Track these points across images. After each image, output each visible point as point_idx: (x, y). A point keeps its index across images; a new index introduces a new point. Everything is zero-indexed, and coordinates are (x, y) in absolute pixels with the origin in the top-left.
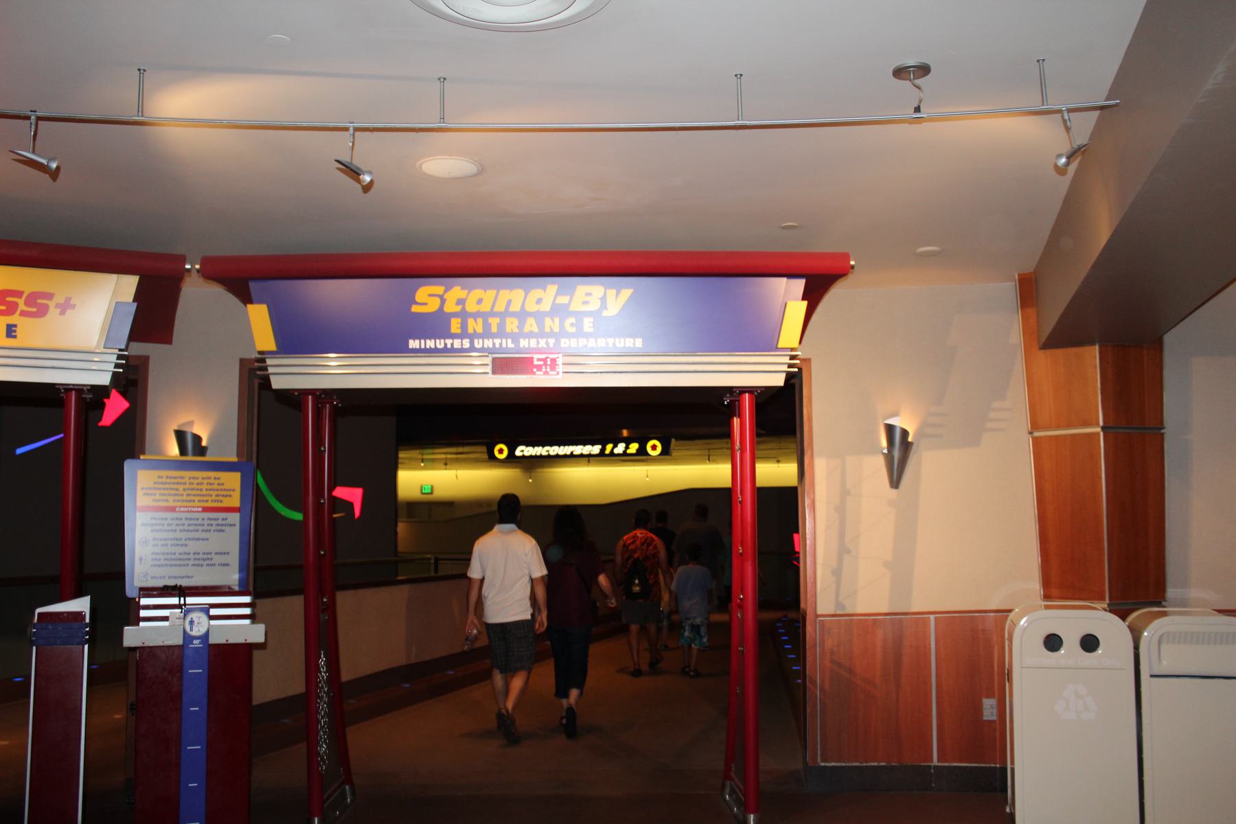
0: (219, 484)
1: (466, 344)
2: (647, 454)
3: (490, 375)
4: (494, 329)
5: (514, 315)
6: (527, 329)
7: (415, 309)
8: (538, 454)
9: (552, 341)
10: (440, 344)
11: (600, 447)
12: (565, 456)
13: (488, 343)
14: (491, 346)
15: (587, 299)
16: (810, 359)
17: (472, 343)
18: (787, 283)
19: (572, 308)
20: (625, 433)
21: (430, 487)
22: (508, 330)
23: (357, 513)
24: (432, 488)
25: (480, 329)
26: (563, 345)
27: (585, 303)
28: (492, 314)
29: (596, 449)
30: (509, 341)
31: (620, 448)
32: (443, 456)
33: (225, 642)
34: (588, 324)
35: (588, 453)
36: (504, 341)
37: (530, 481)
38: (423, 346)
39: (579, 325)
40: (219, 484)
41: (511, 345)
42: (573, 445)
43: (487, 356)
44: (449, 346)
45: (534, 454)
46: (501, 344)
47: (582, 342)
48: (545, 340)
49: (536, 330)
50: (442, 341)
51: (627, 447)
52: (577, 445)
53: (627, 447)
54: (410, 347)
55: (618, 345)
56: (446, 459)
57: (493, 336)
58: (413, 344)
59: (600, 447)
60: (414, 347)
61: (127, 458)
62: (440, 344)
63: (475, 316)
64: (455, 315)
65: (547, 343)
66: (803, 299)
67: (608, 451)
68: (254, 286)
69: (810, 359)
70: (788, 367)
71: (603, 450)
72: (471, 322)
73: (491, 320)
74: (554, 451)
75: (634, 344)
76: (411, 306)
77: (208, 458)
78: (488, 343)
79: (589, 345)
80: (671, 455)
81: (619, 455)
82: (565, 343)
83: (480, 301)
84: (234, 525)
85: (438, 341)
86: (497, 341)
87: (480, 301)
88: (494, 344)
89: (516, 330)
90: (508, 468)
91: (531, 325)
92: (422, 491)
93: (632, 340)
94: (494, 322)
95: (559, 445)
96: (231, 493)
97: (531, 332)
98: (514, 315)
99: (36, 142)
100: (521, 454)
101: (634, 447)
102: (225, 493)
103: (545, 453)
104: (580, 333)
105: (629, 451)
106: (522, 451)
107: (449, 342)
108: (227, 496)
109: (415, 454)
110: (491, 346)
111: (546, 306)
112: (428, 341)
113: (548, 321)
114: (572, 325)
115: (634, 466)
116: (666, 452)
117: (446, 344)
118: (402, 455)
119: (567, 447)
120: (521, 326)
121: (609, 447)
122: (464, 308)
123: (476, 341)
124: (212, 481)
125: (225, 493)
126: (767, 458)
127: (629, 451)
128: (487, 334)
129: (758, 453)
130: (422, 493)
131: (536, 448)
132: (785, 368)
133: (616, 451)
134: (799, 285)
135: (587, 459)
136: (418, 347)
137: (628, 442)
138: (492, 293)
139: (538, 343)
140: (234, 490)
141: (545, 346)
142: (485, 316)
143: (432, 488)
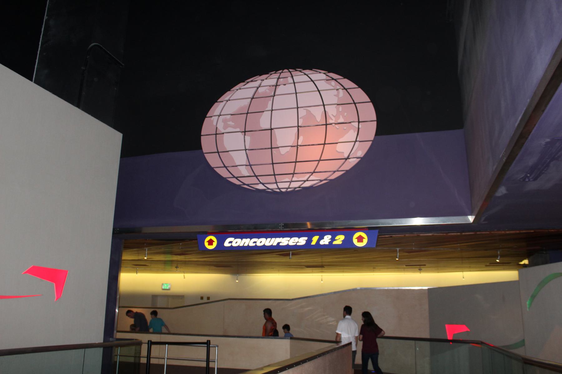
31: (326, 240)
37: (237, 281)
42: (280, 237)
51: (333, 239)
53: (333, 239)
61: (332, 237)
67: (313, 243)
71: (309, 241)
74: (261, 242)
99: (246, 143)
103: (251, 244)
106: (231, 242)
119: (273, 239)
121: (315, 239)
126: (139, 266)
129: (127, 256)
130: (208, 343)
131: (244, 240)
133: (322, 242)
137: (334, 232)
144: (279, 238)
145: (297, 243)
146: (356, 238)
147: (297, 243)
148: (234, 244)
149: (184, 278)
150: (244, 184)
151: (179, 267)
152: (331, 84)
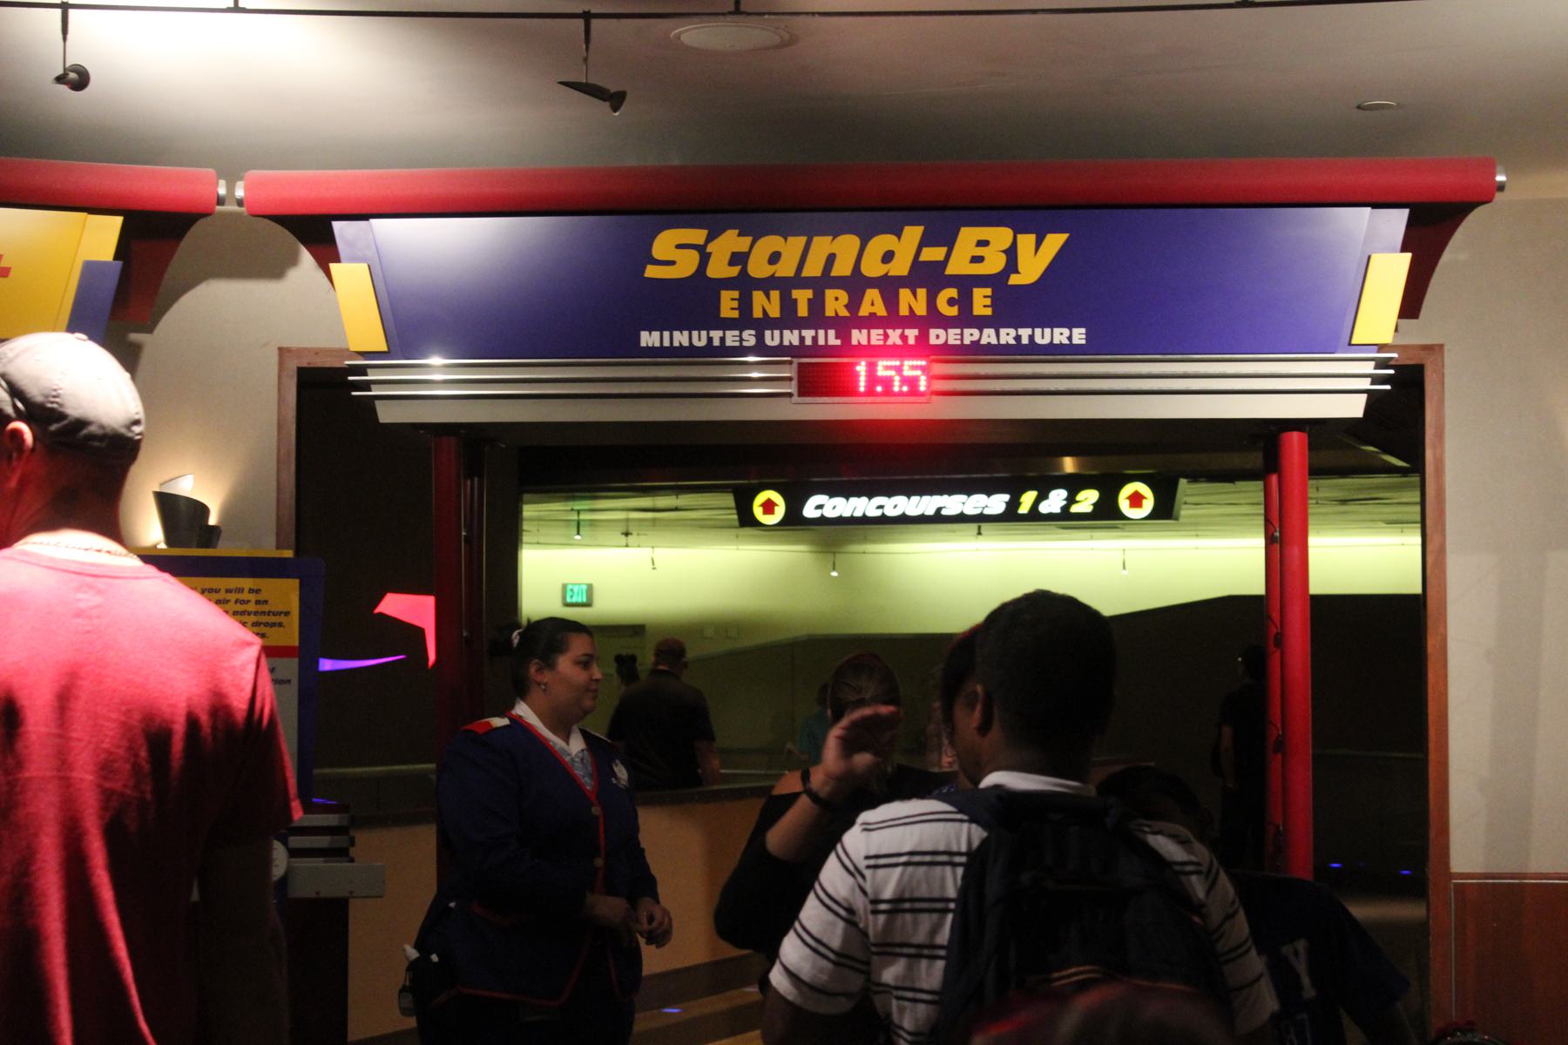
0: (258, 602)
1: (749, 338)
2: (1121, 516)
3: (796, 398)
4: (803, 311)
5: (839, 283)
6: (864, 311)
7: (652, 272)
8: (858, 514)
9: (912, 334)
10: (700, 339)
11: (1006, 497)
12: (922, 520)
13: (791, 337)
14: (796, 342)
15: (980, 251)
16: (1441, 346)
17: (760, 337)
18: (1371, 213)
19: (951, 270)
20: (1069, 465)
21: (585, 587)
22: (829, 312)
24: (590, 588)
25: (775, 311)
26: (933, 341)
27: (977, 259)
28: (799, 281)
29: (997, 503)
30: (832, 333)
31: (1056, 500)
32: (621, 515)
33: (314, 895)
34: (981, 302)
35: (977, 512)
36: (821, 333)
37: (834, 574)
38: (666, 343)
39: (965, 301)
40: (258, 602)
41: (833, 341)
42: (941, 493)
43: (790, 363)
44: (716, 343)
45: (847, 514)
46: (815, 339)
47: (971, 335)
48: (899, 331)
49: (881, 310)
50: (704, 333)
51: (1071, 500)
52: (950, 493)
54: (643, 344)
55: (1038, 340)
56: (627, 520)
57: (800, 324)
58: (649, 339)
59: (1006, 497)
60: (650, 345)
62: (700, 339)
63: (767, 284)
64: (727, 284)
65: (904, 338)
66: (1404, 249)
67: (1024, 509)
68: (342, 230)
69: (1441, 346)
70: (1372, 384)
71: (1013, 505)
72: (758, 297)
73: (796, 294)
75: (1070, 338)
76: (644, 268)
77: (223, 549)
78: (791, 337)
79: (983, 341)
80: (1177, 519)
81: (1051, 517)
82: (938, 337)
83: (775, 258)
84: (289, 681)
85: (695, 333)
86: (808, 334)
87: (775, 258)
88: (802, 339)
89: (844, 313)
90: (780, 542)
91: (873, 302)
92: (564, 597)
93: (1066, 331)
94: (802, 297)
95: (909, 494)
96: (282, 619)
97: (873, 315)
98: (839, 283)
100: (816, 514)
101: (1088, 499)
102: (272, 619)
103: (873, 512)
104: (966, 319)
105: (1075, 509)
106: (820, 507)
107: (716, 335)
108: (273, 625)
109: (555, 508)
110: (796, 342)
111: (900, 267)
112: (676, 334)
113: (905, 295)
114: (951, 302)
115: (1092, 538)
116: (1165, 511)
117: (710, 340)
118: (529, 511)
119: (926, 498)
120: (854, 305)
121: (1028, 499)
122: (744, 271)
123: (768, 333)
124: (245, 596)
125: (272, 619)
127: (1075, 509)
128: (789, 319)
132: (1366, 384)
133: (1044, 508)
134: (1399, 218)
135: (974, 526)
136: (657, 344)
137: (1074, 485)
138: (798, 242)
139: (886, 336)
140: (287, 614)
141: (899, 342)
142: (785, 286)
143: (590, 588)
145: (984, 508)
146: (1127, 498)
147: (984, 508)
148: (829, 513)
149: (1124, 568)
151: (635, 533)
152: (653, 258)
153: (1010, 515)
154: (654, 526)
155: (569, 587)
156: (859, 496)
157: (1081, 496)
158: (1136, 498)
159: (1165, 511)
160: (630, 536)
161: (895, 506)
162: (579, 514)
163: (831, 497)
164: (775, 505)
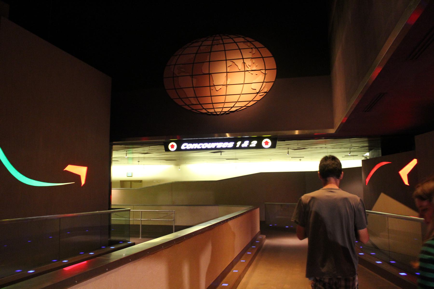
8: (195, 148)
11: (233, 143)
23: (83, 182)
24: (132, 173)
31: (246, 144)
35: (226, 147)
45: (192, 148)
51: (250, 143)
59: (233, 143)
67: (238, 146)
71: (235, 145)
81: (245, 148)
92: (127, 175)
100: (184, 148)
106: (185, 146)
116: (273, 146)
118: (115, 155)
119: (213, 144)
121: (239, 143)
127: (251, 146)
131: (194, 144)
133: (243, 146)
143: (132, 173)
144: (213, 143)
148: (188, 148)
150: (193, 109)
153: (234, 148)
154: (144, 159)
155: (128, 173)
156: (196, 143)
157: (253, 142)
158: (267, 143)
159: (273, 146)
160: (139, 162)
161: (205, 146)
162: (126, 151)
163: (188, 144)
164: (174, 146)
